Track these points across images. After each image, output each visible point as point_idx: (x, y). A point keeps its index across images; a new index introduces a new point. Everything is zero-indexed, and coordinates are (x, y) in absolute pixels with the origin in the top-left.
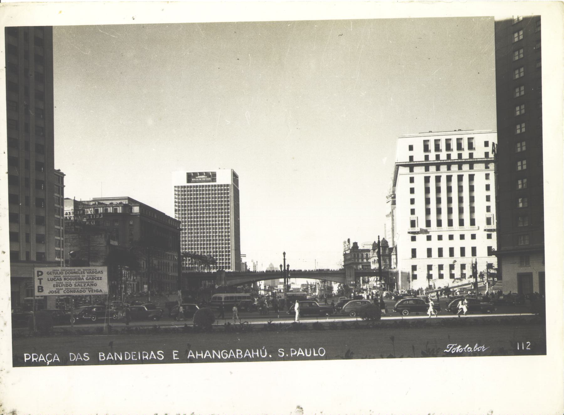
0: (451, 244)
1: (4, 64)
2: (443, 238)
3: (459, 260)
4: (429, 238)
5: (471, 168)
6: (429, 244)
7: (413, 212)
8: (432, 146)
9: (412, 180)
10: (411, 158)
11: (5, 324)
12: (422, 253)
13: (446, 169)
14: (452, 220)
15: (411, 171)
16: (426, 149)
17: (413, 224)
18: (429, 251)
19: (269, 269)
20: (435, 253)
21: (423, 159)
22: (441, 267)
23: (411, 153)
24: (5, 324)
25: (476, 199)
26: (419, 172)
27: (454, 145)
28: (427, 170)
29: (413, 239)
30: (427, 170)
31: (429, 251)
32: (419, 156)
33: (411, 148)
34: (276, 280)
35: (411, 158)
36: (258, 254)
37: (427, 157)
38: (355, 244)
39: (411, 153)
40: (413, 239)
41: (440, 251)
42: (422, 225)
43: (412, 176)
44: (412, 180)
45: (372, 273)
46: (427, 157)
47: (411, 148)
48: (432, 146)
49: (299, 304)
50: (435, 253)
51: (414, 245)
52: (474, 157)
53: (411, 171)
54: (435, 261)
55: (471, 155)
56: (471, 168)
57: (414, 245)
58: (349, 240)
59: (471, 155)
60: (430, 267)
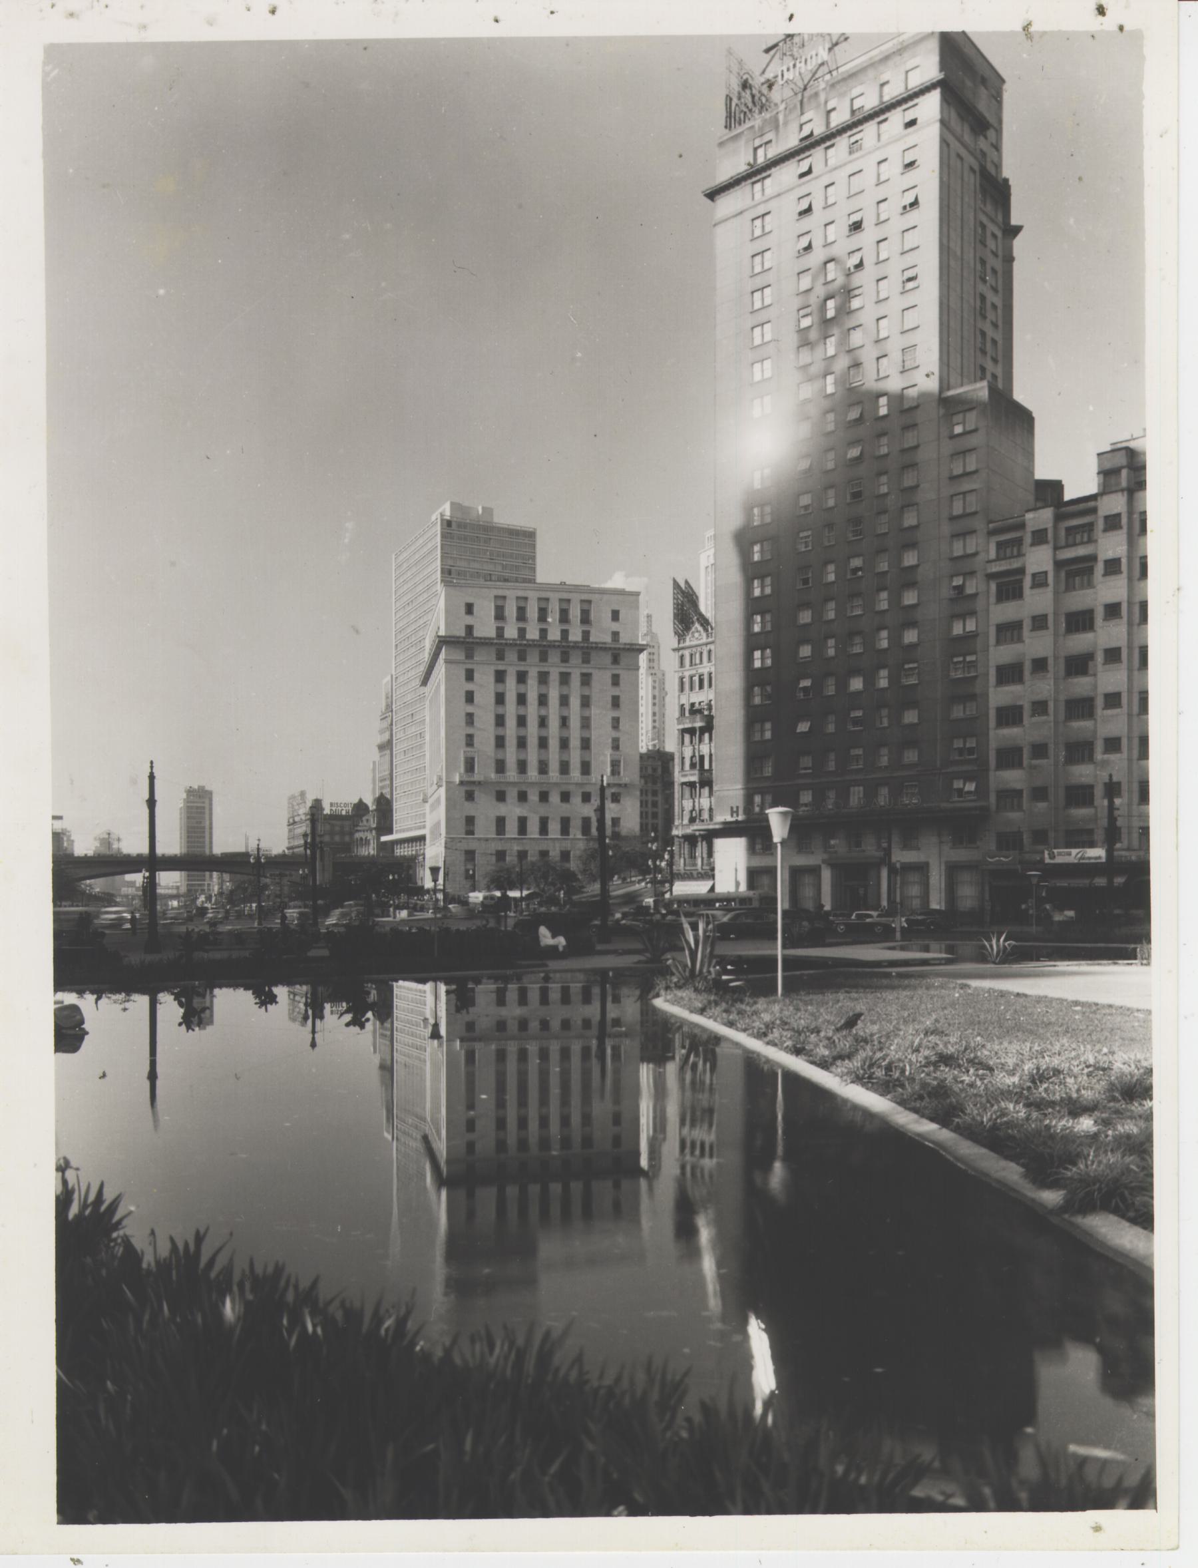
0: (564, 809)
5: (586, 660)
10: (469, 629)
11: (72, 15)
13: (537, 660)
15: (470, 656)
19: (104, 851)
23: (469, 620)
24: (72, 15)
25: (593, 724)
28: (500, 656)
29: (470, 796)
30: (500, 656)
32: (486, 628)
34: (118, 878)
35: (469, 629)
37: (500, 631)
38: (317, 805)
39: (469, 620)
45: (605, 890)
46: (500, 631)
47: (469, 609)
52: (592, 639)
53: (470, 656)
55: (586, 635)
56: (586, 660)
58: (303, 794)
59: (586, 635)
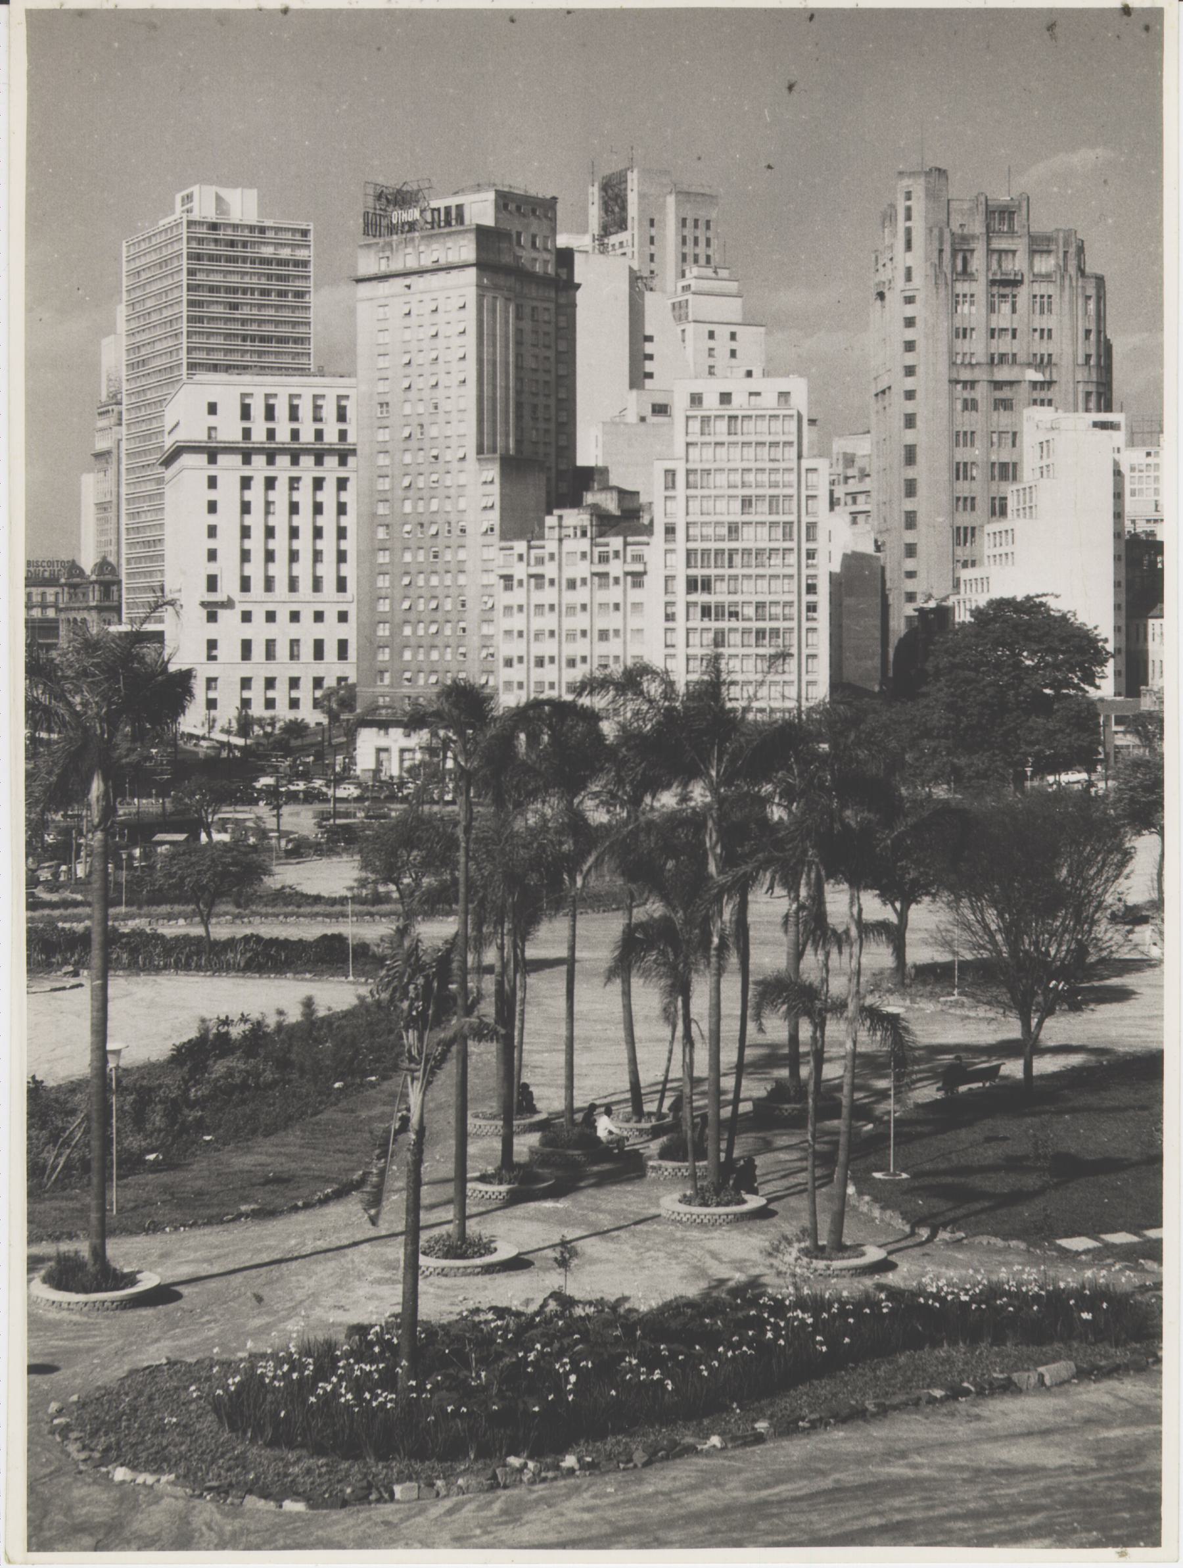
0: (294, 631)
1: (626, 5)
2: (302, 617)
3: (283, 669)
4: (246, 617)
6: (247, 631)
7: (212, 555)
8: (258, 411)
9: (212, 482)
12: (229, 651)
14: (345, 578)
15: (212, 460)
16: (246, 413)
17: (212, 583)
18: (246, 646)
20: (258, 651)
21: (238, 436)
22: (294, 683)
23: (212, 421)
26: (230, 465)
27: (282, 411)
28: (247, 461)
30: (247, 461)
31: (246, 646)
33: (212, 409)
36: (1151, 622)
37: (247, 433)
40: (212, 617)
41: (319, 647)
42: (229, 587)
43: (212, 473)
44: (212, 482)
46: (247, 433)
47: (212, 409)
48: (258, 411)
49: (105, 780)
50: (258, 651)
51: (212, 630)
53: (212, 460)
54: (258, 669)
57: (212, 630)
60: (246, 683)
